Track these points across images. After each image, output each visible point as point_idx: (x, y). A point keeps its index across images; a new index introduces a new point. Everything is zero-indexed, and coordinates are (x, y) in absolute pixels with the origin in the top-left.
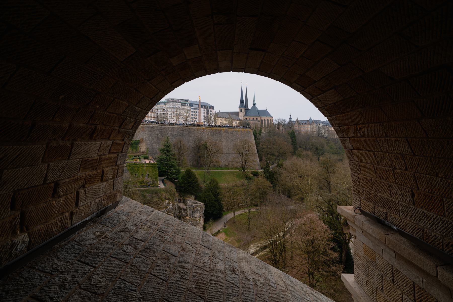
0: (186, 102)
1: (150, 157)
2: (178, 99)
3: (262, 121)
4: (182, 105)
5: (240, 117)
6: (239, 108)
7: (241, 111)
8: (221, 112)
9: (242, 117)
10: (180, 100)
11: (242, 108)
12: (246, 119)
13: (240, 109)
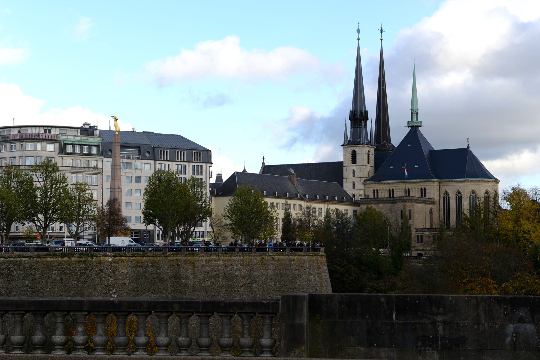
0: (86, 139)
1: (184, 303)
2: (48, 129)
3: (447, 199)
4: (62, 150)
5: (347, 186)
6: (347, 144)
7: (354, 161)
8: (269, 167)
9: (360, 186)
10: (54, 132)
11: (359, 144)
12: (376, 192)
13: (350, 150)
